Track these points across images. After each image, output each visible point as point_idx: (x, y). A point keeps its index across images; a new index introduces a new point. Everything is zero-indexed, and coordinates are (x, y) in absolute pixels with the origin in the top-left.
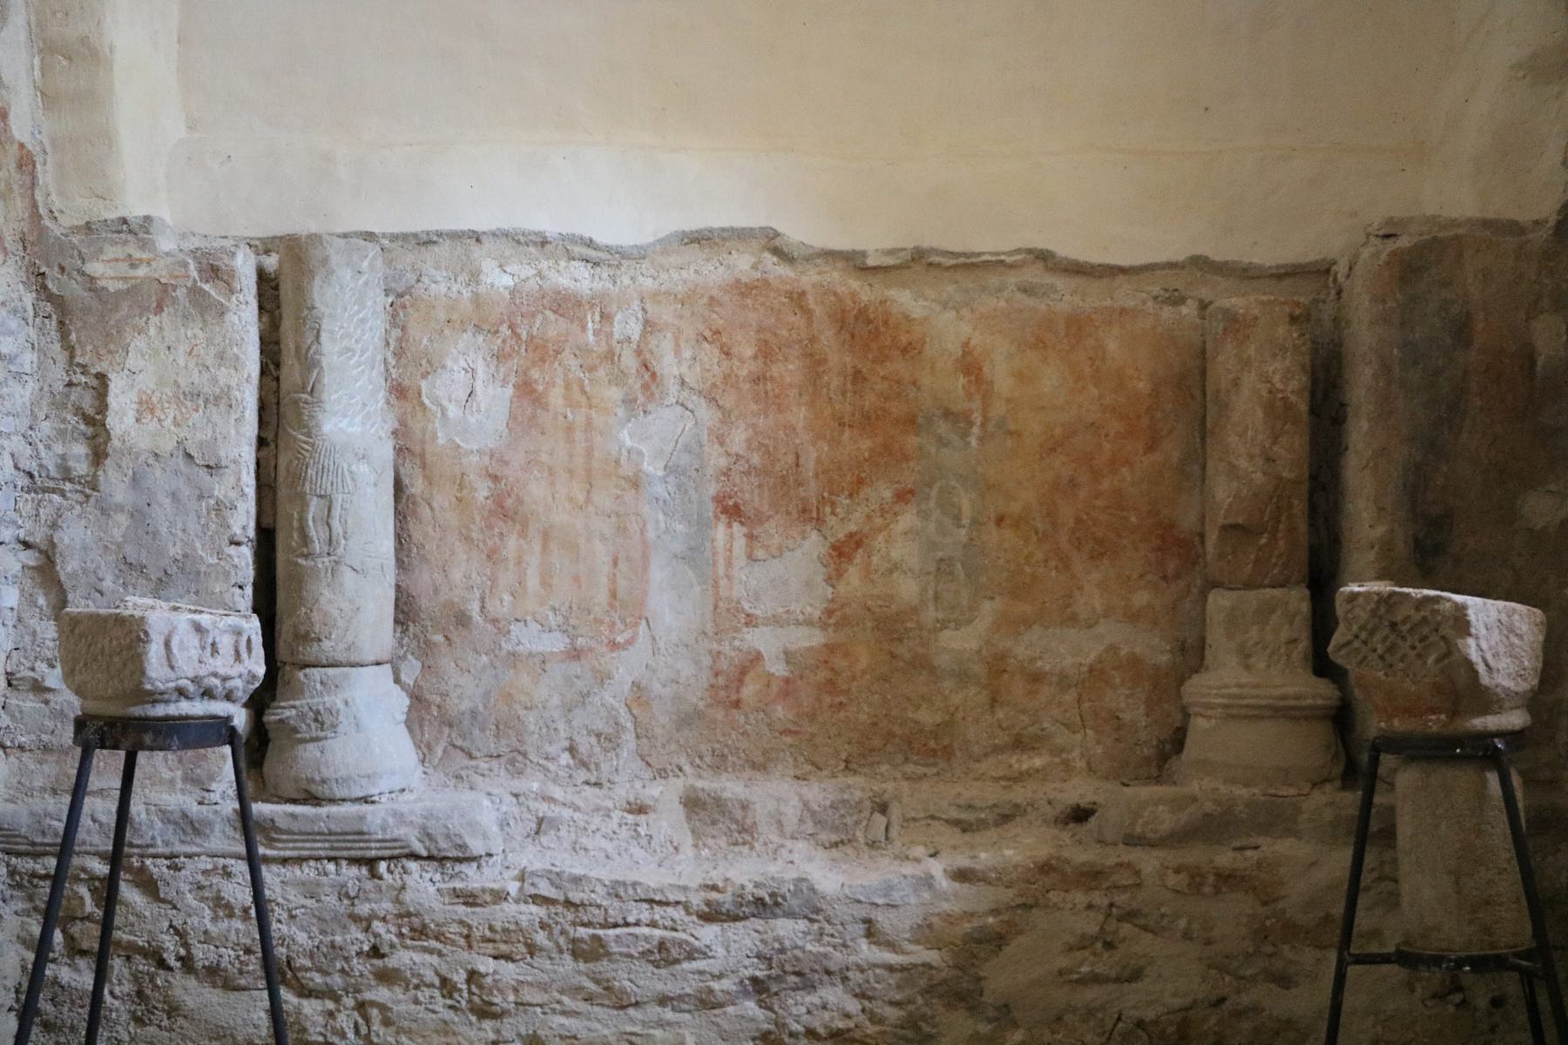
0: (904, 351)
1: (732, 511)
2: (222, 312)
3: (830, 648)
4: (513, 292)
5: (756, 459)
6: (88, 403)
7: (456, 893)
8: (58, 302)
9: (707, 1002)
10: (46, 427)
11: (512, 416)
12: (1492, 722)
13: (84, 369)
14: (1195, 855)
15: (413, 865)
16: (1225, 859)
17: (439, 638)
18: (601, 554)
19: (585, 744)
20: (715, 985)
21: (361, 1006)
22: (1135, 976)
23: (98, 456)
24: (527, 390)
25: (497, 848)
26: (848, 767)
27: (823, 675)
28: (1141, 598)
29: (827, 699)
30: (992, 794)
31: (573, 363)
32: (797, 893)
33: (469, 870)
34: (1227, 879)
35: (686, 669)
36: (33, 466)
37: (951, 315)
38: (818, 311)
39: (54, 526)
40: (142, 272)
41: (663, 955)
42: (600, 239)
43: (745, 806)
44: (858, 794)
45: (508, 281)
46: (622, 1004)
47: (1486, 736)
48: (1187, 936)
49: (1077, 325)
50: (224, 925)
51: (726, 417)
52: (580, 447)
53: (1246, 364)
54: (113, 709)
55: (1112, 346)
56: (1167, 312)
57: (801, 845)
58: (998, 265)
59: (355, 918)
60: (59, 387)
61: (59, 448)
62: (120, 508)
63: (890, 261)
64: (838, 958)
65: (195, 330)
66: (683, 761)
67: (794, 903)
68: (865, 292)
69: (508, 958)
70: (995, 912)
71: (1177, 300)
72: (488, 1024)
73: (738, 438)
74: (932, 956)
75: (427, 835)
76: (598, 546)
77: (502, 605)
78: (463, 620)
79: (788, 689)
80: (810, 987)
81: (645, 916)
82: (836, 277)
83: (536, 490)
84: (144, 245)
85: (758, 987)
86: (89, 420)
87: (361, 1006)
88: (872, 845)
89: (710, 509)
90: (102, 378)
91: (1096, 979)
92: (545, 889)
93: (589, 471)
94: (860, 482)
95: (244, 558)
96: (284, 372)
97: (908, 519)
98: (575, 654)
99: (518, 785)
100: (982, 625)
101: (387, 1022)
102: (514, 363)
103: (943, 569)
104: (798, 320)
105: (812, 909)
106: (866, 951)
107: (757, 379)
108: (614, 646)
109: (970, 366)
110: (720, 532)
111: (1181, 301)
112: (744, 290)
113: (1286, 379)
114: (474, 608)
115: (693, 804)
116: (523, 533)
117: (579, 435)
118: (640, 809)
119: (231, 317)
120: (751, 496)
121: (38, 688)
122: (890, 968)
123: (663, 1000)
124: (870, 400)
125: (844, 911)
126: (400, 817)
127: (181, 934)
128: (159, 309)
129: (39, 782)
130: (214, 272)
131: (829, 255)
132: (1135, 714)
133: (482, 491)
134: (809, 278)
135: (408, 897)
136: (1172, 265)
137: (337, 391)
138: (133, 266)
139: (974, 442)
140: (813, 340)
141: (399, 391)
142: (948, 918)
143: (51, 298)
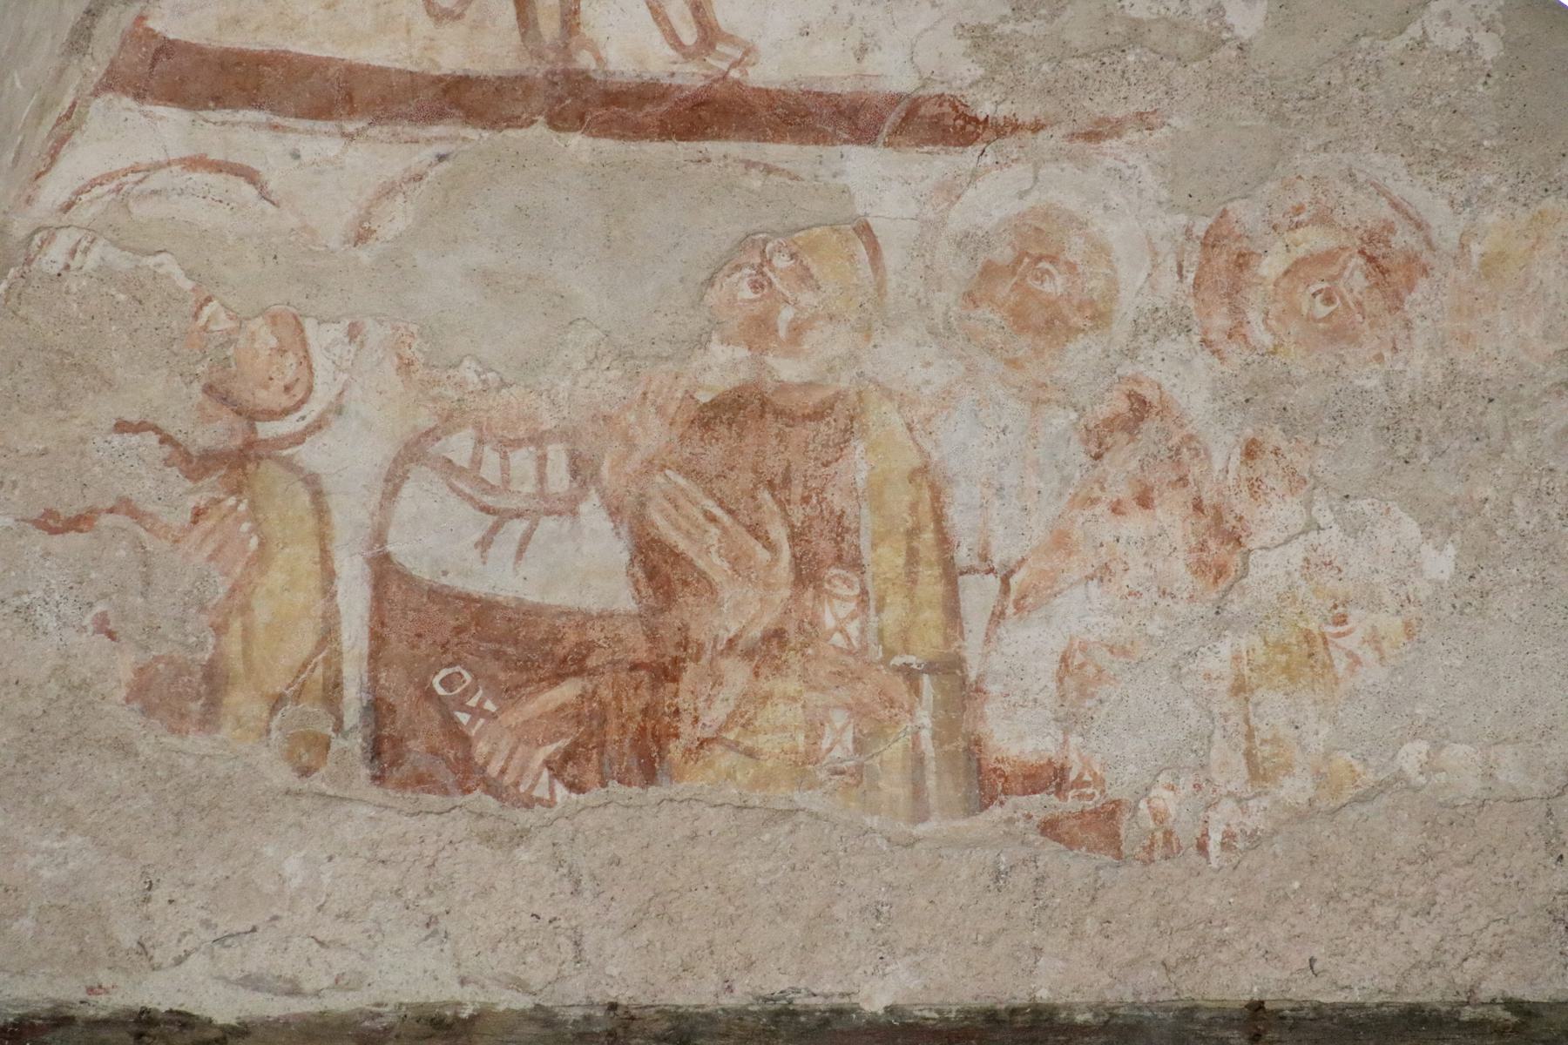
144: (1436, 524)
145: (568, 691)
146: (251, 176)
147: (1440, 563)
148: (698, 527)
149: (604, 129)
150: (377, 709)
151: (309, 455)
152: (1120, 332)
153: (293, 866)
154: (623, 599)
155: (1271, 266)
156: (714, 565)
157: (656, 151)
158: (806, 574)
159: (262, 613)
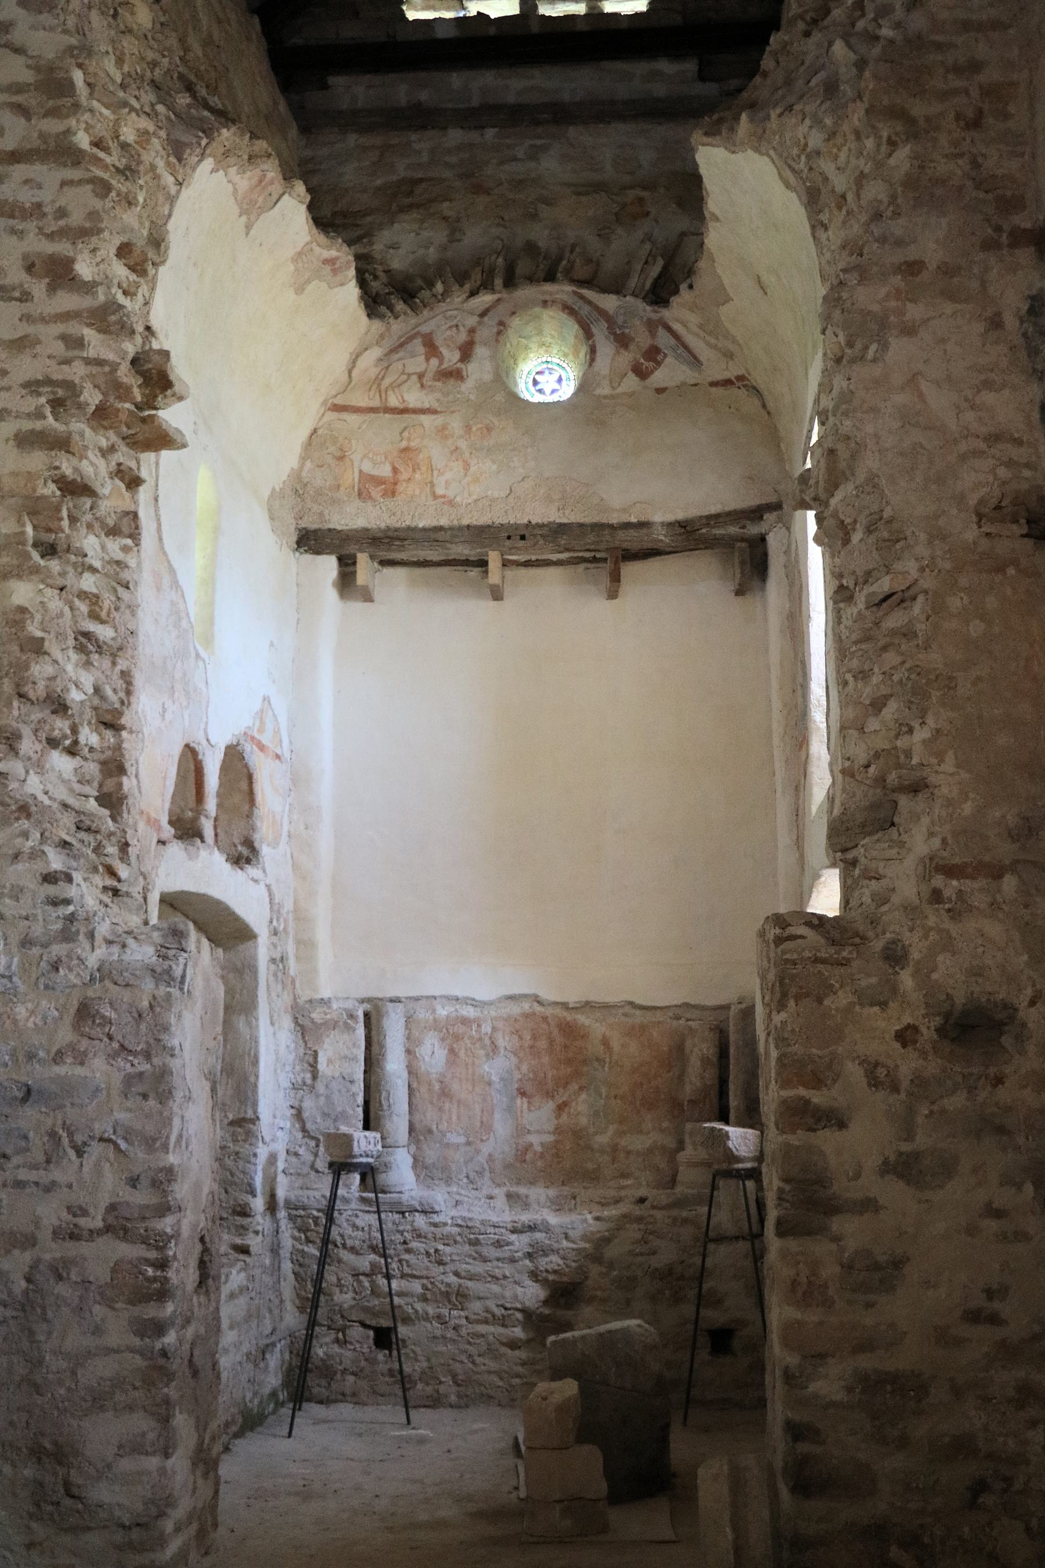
0: (583, 1037)
1: (523, 1094)
2: (354, 1030)
3: (557, 1142)
4: (448, 1017)
5: (531, 1076)
6: (311, 1060)
7: (431, 1223)
8: (302, 1027)
9: (513, 1260)
10: (298, 1068)
11: (447, 1061)
12: (740, 1166)
13: (310, 1049)
14: (675, 1212)
15: (417, 1214)
16: (684, 1214)
17: (422, 1138)
18: (478, 1109)
19: (472, 1175)
20: (516, 1255)
21: (400, 1261)
22: (654, 1253)
23: (315, 1077)
24: (452, 1051)
25: (443, 1209)
26: (563, 1184)
27: (554, 1151)
28: (665, 1124)
29: (556, 1160)
30: (612, 1193)
31: (468, 1042)
32: (542, 1223)
33: (435, 1216)
34: (685, 1221)
35: (507, 1149)
36: (294, 1081)
37: (598, 1024)
38: (552, 1023)
39: (301, 1101)
40: (328, 1017)
41: (498, 1244)
42: (477, 998)
43: (527, 1197)
44: (566, 1193)
45: (445, 1013)
46: (485, 1260)
47: (738, 1170)
48: (671, 1239)
49: (643, 1028)
50: (356, 1233)
51: (521, 1061)
52: (470, 1071)
53: (694, 1046)
54: (342, 1160)
55: (655, 1034)
56: (675, 1023)
57: (545, 1210)
58: (614, 1007)
59: (398, 1231)
60: (302, 1055)
61: (302, 1075)
62: (322, 1095)
63: (578, 1005)
64: (556, 1246)
65: (346, 1036)
66: (506, 1181)
67: (541, 1227)
68: (569, 1017)
69: (448, 1245)
70: (608, 1231)
71: (678, 1018)
72: (441, 1267)
73: (524, 1068)
74: (587, 1245)
75: (421, 1204)
76: (477, 1106)
77: (444, 1126)
78: (430, 1131)
79: (542, 1156)
80: (546, 1255)
81: (492, 1231)
82: (559, 1011)
83: (455, 1086)
84: (329, 1007)
85: (529, 1256)
86: (311, 1066)
87: (400, 1261)
88: (570, 1210)
89: (515, 1093)
90: (316, 1052)
91: (641, 1254)
92: (460, 1222)
93: (473, 1080)
94: (567, 1083)
95: (360, 1110)
96: (373, 1048)
97: (584, 1096)
98: (468, 1143)
99: (449, 1189)
100: (610, 1133)
101: (408, 1266)
102: (448, 1041)
103: (596, 1114)
104: (544, 1026)
105: (547, 1229)
106: (565, 1244)
107: (531, 1047)
108: (482, 1140)
109: (605, 1042)
110: (519, 1101)
111: (680, 1018)
112: (527, 1016)
113: (708, 1049)
114: (434, 1127)
115: (509, 1196)
116: (451, 1102)
117: (470, 1067)
118: (491, 1198)
119: (357, 1031)
120: (529, 1088)
121: (296, 1154)
122: (573, 1250)
123: (498, 1260)
124: (570, 1055)
125: (558, 1230)
126: (412, 1197)
127: (342, 1236)
128: (334, 1029)
129: (297, 1185)
130: (351, 1016)
131: (556, 1003)
132: (663, 1165)
133: (437, 1087)
134: (549, 1011)
135: (415, 1224)
136: (676, 1006)
137: (19, 708)
138: (326, 1014)
139: (606, 1069)
140: (550, 1033)
141: (408, 1052)
142: (592, 1233)
143: (299, 1025)
144: (494, 462)
147: (494, 467)
150: (359, 490)
154: (391, 475)
156: (402, 470)
158: (414, 471)
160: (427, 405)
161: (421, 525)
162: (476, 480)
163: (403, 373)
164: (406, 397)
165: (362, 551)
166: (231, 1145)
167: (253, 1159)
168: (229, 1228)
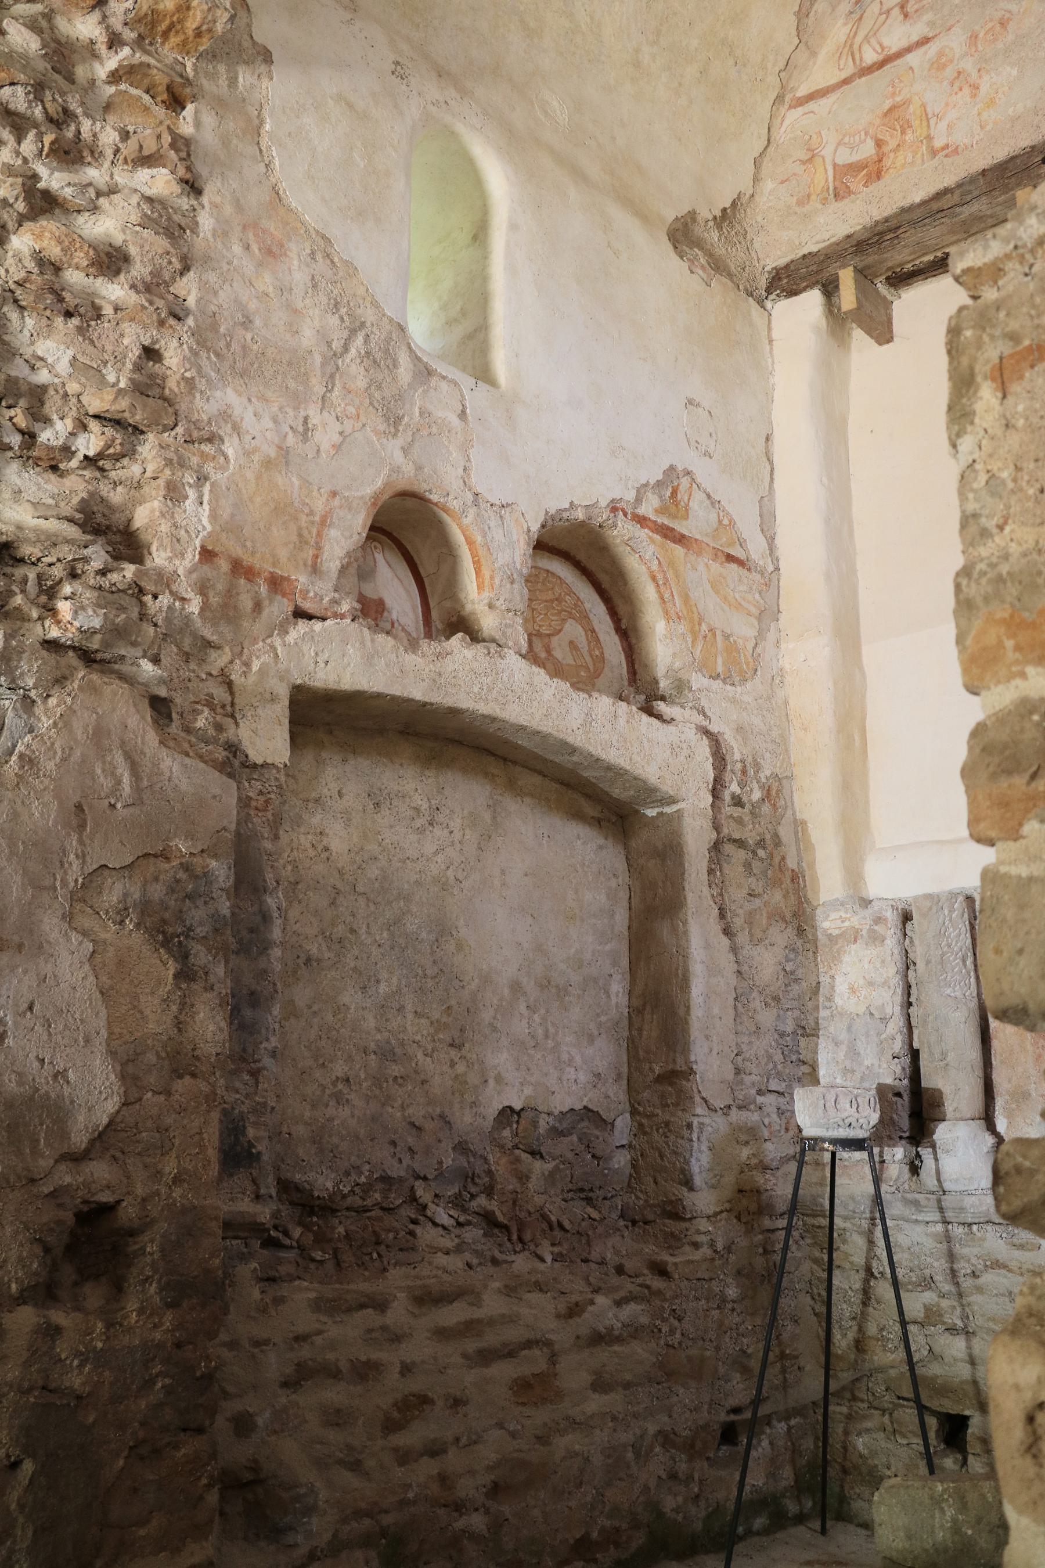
40: (847, 924)
128: (855, 941)
145: (865, 172)
146: (812, 112)
148: (707, 1037)
149: (868, 74)
150: (835, 188)
151: (822, 153)
152: (955, 62)
153: (822, 221)
155: (981, 35)
157: (876, 74)
158: (903, 132)
159: (816, 181)
160: (915, 38)
161: (917, 200)
162: (991, 103)
163: (881, 14)
164: (886, 42)
165: (844, 266)
166: (660, 1112)
167: (685, 1132)
168: (655, 1236)
